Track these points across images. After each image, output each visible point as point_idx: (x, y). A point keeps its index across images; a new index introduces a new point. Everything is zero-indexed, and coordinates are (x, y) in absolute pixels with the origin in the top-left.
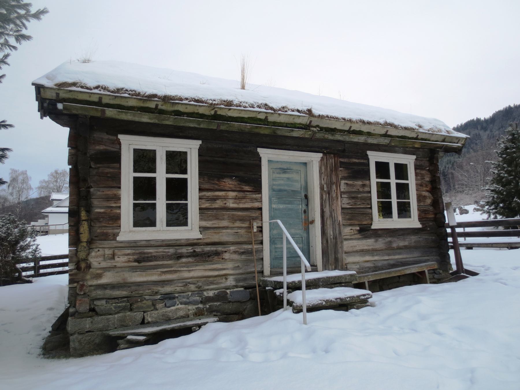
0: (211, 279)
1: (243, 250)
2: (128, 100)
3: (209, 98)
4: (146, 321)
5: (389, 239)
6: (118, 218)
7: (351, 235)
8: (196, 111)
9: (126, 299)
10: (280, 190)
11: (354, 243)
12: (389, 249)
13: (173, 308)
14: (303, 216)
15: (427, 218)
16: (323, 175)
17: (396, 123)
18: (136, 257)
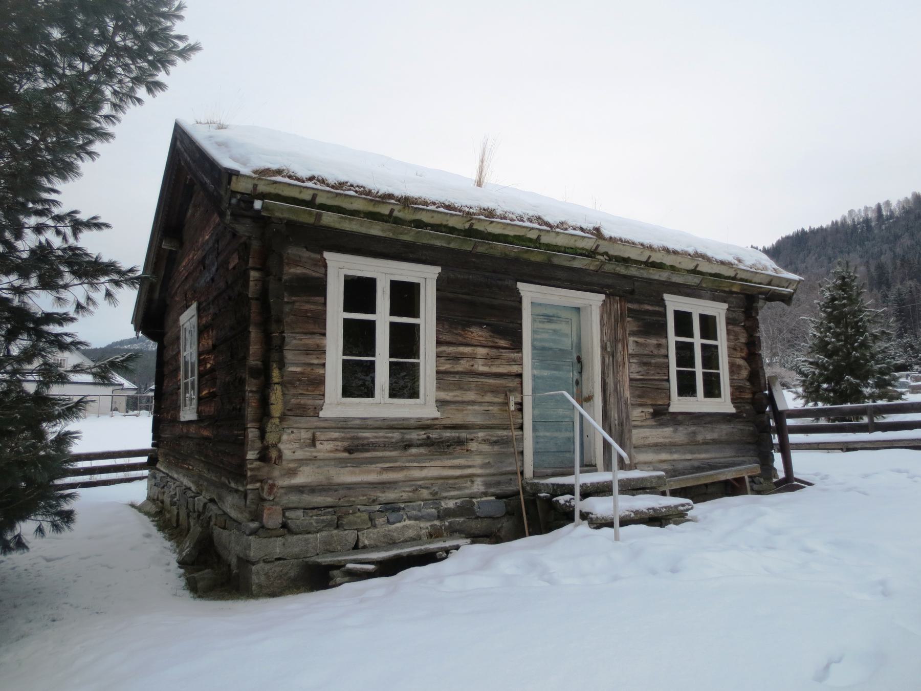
0: (451, 481)
1: (495, 439)
2: (353, 200)
3: (464, 204)
4: (361, 545)
5: (693, 428)
6: (319, 382)
7: (642, 421)
8: (444, 223)
9: (330, 510)
11: (646, 432)
12: (693, 444)
14: (575, 390)
16: (605, 328)
18: (346, 444)
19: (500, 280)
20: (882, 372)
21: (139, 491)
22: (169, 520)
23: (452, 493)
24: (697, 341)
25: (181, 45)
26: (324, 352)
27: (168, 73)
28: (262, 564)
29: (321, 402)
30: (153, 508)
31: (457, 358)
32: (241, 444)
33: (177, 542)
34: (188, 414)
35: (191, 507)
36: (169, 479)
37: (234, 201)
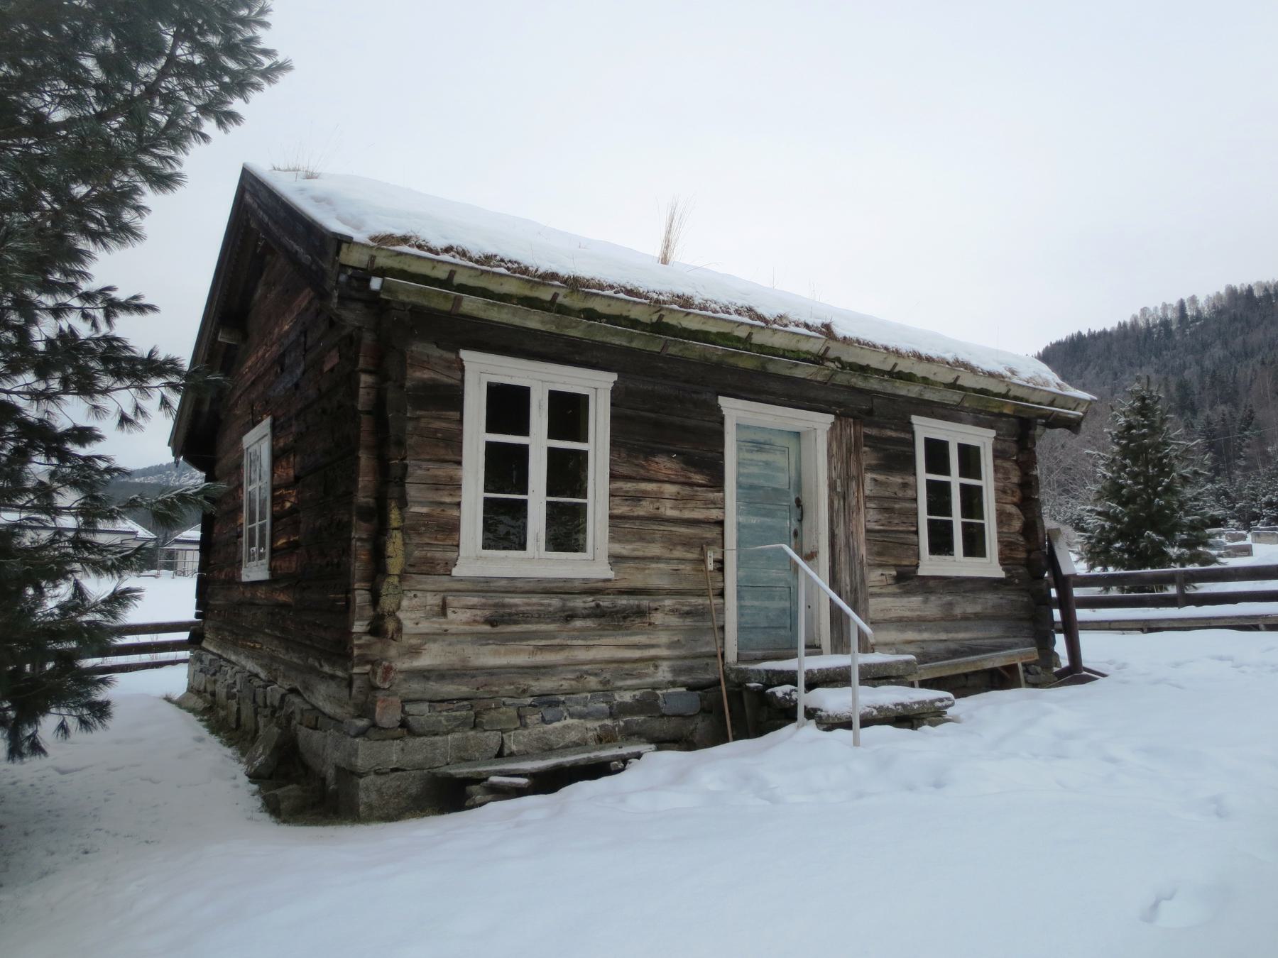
0: (626, 666)
2: (504, 280)
3: (651, 289)
4: (506, 751)
5: (949, 598)
6: (452, 528)
8: (625, 314)
9: (465, 703)
10: (752, 487)
11: (888, 602)
12: (949, 620)
13: (557, 724)
15: (1014, 559)
16: (834, 460)
17: (974, 363)
18: (487, 613)
19: (695, 392)
20: (1193, 527)
21: (176, 679)
22: (225, 719)
23: (629, 682)
24: (955, 480)
25: (267, 62)
26: (459, 487)
27: (246, 101)
28: (372, 777)
29: (454, 555)
30: (200, 704)
31: (637, 498)
32: (346, 610)
33: (240, 749)
34: (255, 571)
35: (260, 700)
36: (223, 663)
37: (343, 278)
